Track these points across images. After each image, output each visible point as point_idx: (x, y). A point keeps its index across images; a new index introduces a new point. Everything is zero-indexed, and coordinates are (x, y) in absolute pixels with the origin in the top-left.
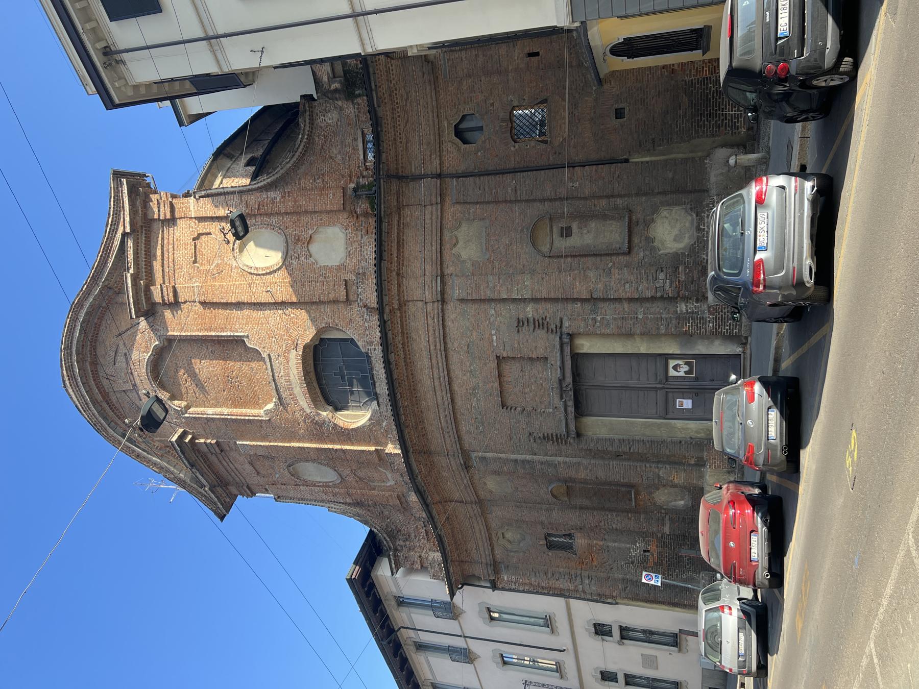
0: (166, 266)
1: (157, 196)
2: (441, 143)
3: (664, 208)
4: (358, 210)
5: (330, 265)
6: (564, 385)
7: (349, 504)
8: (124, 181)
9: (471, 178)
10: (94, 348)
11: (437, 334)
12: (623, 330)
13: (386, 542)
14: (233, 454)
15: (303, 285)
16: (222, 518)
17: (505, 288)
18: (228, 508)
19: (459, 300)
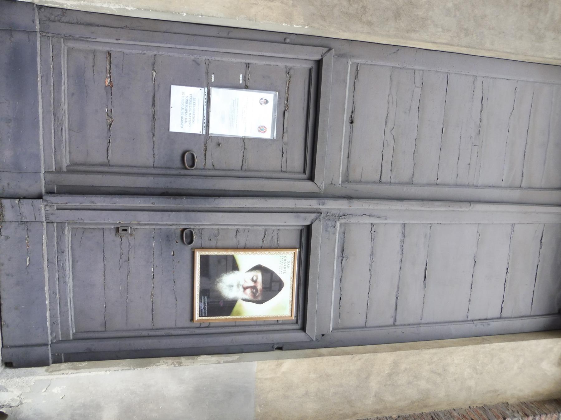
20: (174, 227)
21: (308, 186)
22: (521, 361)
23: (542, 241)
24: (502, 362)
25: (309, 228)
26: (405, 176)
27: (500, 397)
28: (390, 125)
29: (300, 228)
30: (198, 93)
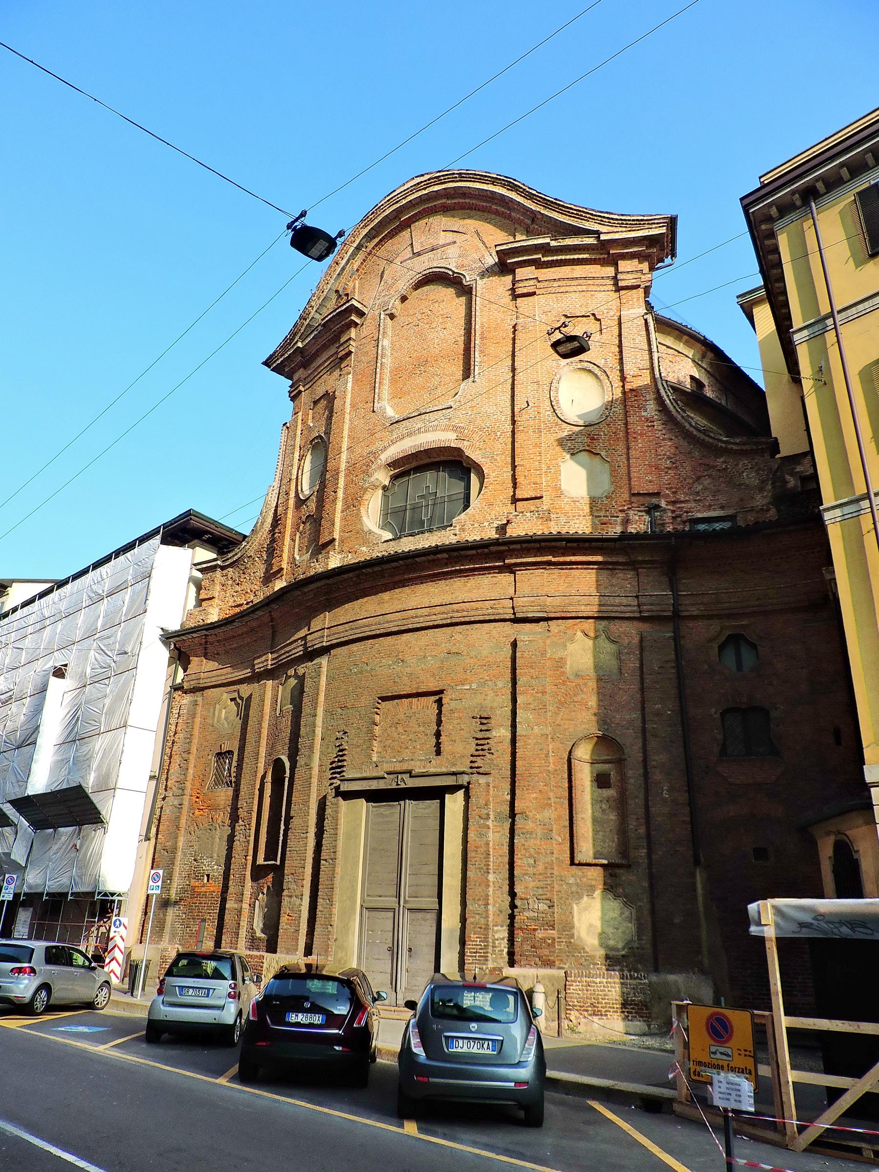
0: (560, 283)
1: (646, 270)
2: (719, 617)
3: (634, 911)
4: (631, 512)
5: (562, 477)
7: (276, 511)
8: (663, 230)
9: (673, 656)
10: (462, 207)
11: (472, 613)
13: (234, 555)
14: (337, 373)
15: (536, 446)
16: (266, 363)
17: (531, 700)
18: (278, 370)
19: (515, 640)
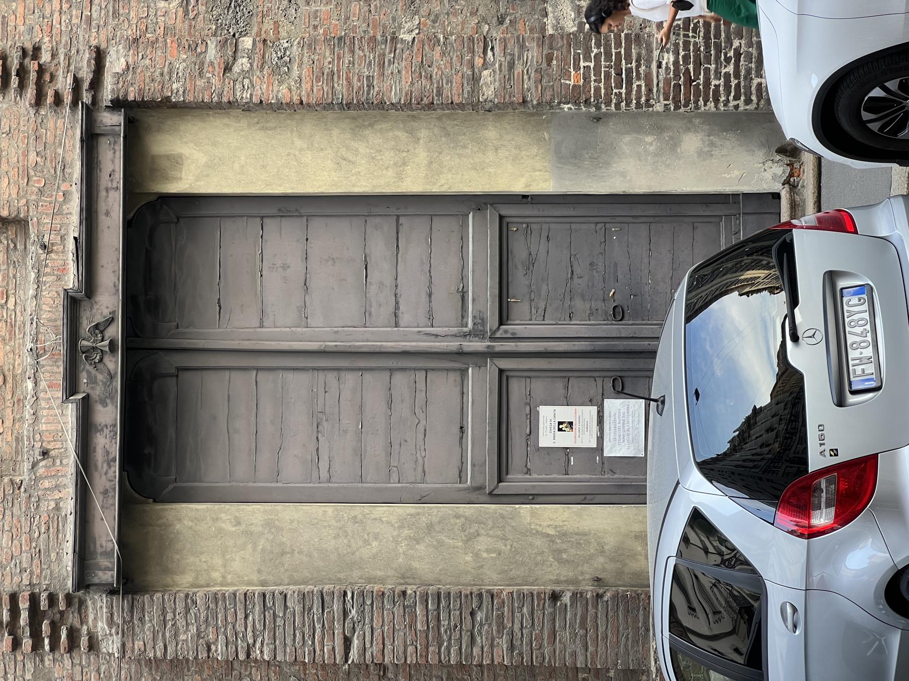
6: (86, 326)
12: (341, 88)
20: (630, 322)
21: (505, 364)
22: (237, 166)
23: (218, 308)
24: (264, 167)
25: (501, 323)
26: (398, 378)
27: (256, 120)
28: (421, 428)
29: (509, 322)
30: (611, 450)
